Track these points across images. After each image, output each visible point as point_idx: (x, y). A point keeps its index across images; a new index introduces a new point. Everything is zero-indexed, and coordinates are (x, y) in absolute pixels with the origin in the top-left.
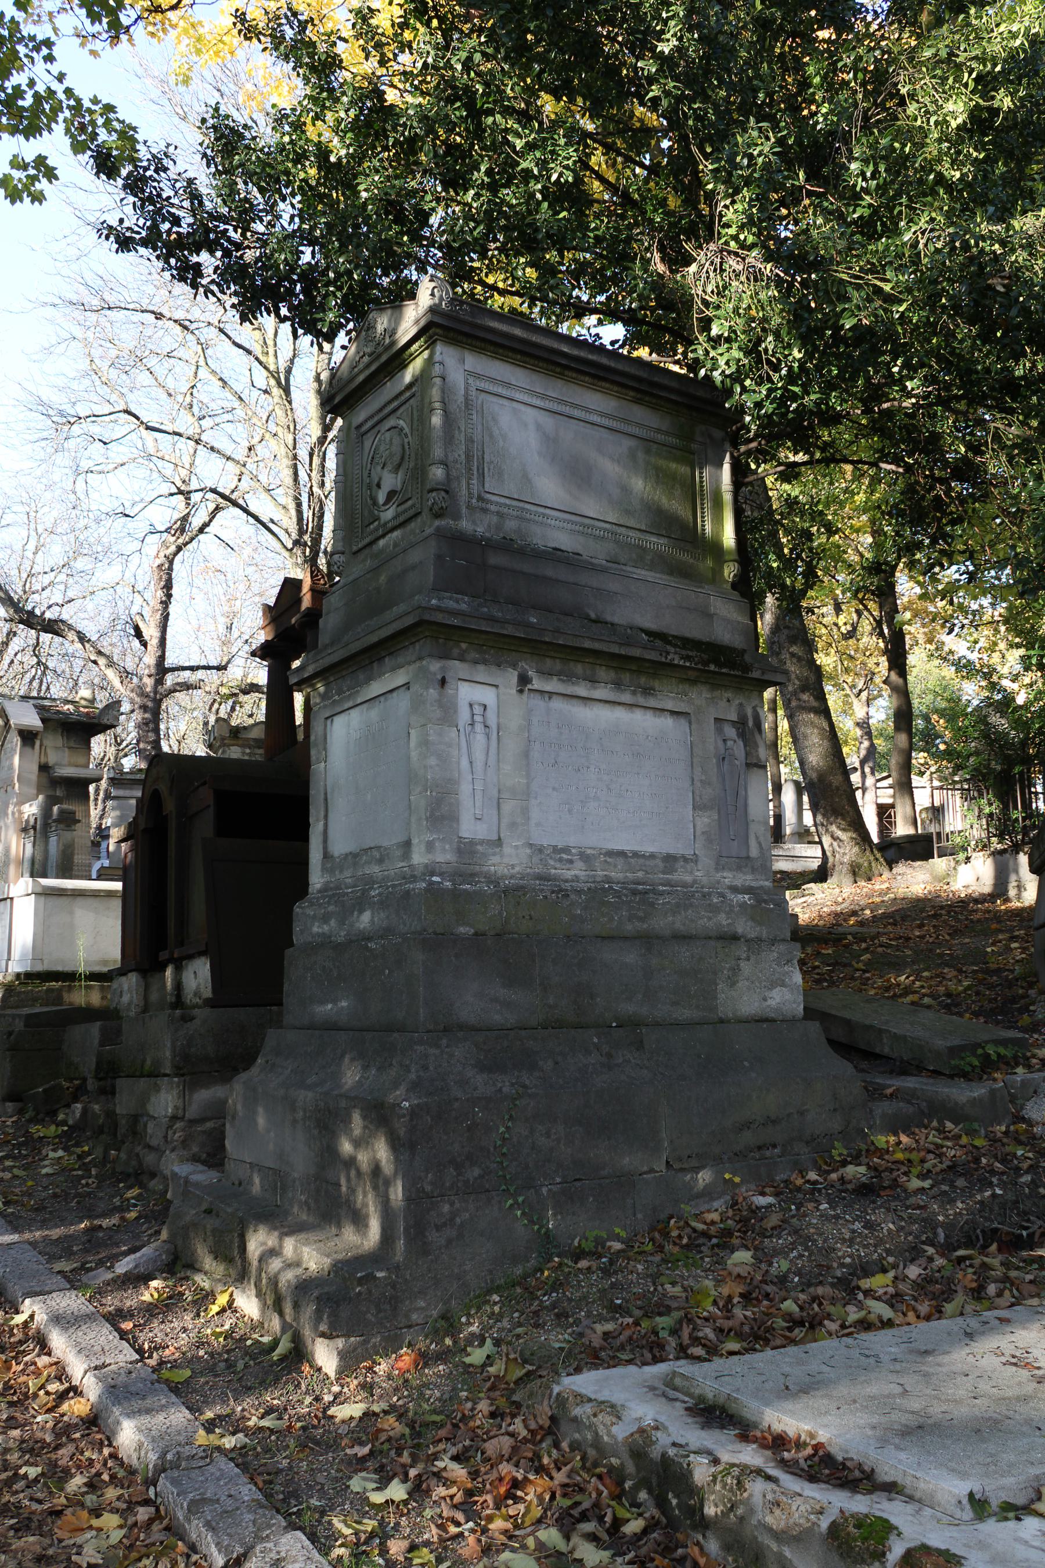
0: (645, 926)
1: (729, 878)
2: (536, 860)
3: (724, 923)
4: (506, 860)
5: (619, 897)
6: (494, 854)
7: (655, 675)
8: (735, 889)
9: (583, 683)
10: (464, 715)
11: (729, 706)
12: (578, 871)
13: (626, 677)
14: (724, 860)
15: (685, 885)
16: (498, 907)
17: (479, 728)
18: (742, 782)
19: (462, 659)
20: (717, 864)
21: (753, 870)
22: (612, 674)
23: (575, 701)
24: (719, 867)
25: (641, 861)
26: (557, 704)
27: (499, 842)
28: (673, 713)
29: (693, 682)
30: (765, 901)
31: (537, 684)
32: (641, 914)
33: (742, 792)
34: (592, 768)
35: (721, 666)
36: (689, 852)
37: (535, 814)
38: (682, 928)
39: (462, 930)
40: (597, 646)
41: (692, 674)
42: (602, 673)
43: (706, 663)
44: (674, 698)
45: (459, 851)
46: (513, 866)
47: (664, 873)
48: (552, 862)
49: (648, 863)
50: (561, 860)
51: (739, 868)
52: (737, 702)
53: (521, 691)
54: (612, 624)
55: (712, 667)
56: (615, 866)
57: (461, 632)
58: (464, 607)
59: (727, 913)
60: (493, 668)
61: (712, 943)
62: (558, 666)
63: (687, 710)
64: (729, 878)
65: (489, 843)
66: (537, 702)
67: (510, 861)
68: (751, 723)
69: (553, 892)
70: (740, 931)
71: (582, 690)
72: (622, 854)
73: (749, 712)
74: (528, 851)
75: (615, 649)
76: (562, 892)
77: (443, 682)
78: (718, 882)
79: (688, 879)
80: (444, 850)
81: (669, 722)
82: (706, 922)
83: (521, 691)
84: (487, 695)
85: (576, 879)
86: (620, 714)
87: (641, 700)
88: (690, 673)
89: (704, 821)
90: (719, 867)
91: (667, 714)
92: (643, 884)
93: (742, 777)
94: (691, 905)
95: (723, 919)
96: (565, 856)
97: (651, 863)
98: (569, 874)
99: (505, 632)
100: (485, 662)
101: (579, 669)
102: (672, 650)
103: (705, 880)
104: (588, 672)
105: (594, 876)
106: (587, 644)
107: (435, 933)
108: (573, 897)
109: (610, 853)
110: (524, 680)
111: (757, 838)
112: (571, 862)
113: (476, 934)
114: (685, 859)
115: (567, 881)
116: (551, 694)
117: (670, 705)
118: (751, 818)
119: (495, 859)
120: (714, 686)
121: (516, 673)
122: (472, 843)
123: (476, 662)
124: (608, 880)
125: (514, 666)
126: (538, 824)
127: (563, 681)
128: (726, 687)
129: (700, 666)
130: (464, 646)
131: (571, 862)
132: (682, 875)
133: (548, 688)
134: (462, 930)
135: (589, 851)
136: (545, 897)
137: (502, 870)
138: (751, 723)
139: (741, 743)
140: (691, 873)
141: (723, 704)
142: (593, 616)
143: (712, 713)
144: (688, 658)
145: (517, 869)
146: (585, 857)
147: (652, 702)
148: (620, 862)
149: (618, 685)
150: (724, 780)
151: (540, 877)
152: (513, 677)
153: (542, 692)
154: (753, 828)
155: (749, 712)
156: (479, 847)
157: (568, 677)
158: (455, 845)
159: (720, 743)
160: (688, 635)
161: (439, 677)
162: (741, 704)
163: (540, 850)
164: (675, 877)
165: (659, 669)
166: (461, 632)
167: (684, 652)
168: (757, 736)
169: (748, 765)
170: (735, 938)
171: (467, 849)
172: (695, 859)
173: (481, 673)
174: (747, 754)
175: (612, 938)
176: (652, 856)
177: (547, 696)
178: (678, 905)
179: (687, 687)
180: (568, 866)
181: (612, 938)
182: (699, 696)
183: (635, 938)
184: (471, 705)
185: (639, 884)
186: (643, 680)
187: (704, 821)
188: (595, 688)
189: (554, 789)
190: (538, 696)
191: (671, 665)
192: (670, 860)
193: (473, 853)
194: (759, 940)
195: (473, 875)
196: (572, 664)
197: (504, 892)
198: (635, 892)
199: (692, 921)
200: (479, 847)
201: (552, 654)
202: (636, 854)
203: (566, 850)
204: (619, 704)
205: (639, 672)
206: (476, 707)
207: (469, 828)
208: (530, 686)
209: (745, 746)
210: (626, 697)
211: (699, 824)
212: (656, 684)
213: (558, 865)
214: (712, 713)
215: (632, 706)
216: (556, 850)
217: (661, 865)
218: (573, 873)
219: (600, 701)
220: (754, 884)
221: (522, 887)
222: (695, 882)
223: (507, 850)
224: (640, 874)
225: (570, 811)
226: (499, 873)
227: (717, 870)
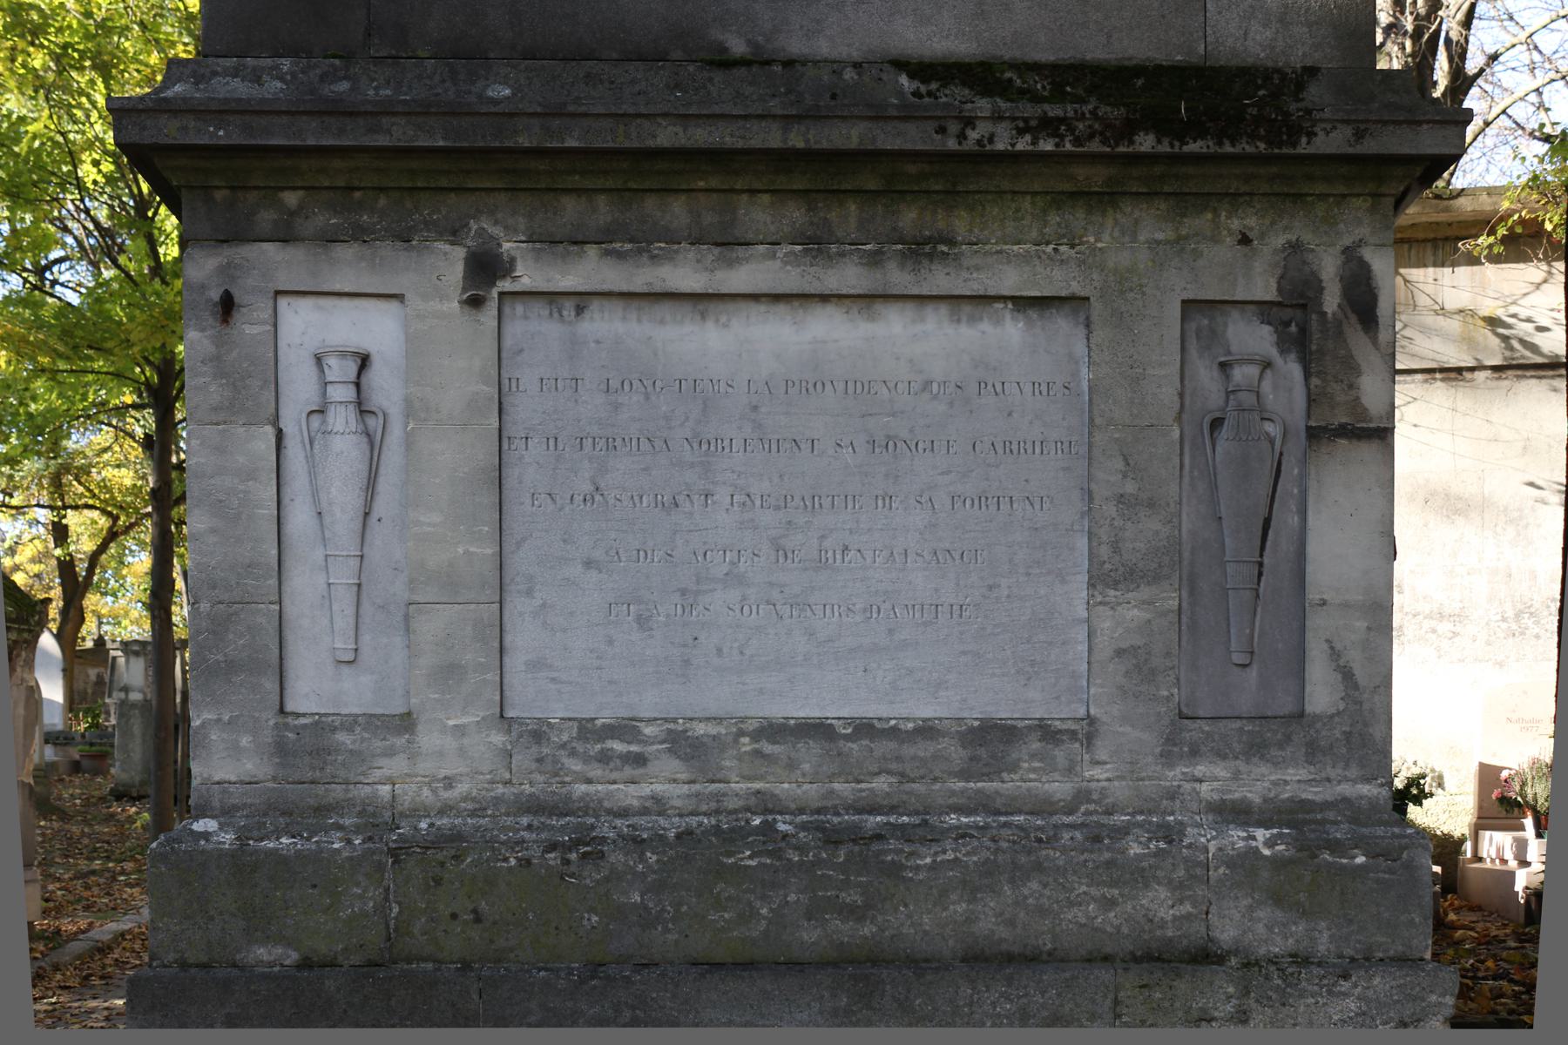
0: (867, 930)
1: (1213, 779)
2: (522, 760)
3: (1166, 913)
4: (425, 767)
5: (776, 854)
6: (390, 753)
7: (952, 197)
8: (1234, 813)
9: (691, 253)
10: (299, 388)
11: (1241, 260)
12: (667, 781)
13: (848, 217)
14: (1194, 731)
15: (1044, 807)
16: (375, 893)
17: (342, 419)
18: (1287, 484)
19: (285, 237)
20: (1170, 740)
21: (1313, 752)
22: (796, 214)
23: (665, 309)
24: (1175, 747)
25: (885, 747)
26: (603, 324)
27: (406, 722)
28: (1022, 303)
29: (1103, 199)
30: (1336, 847)
31: (528, 275)
32: (853, 897)
33: (1285, 519)
34: (722, 495)
35: (1181, 132)
36: (1064, 711)
37: (524, 637)
38: (1003, 932)
39: (262, 953)
40: (701, 136)
41: (1095, 177)
42: (757, 215)
43: (1128, 130)
44: (1026, 258)
45: (281, 750)
46: (449, 782)
47: (965, 775)
48: (575, 766)
49: (908, 750)
50: (605, 758)
51: (1256, 749)
52: (1279, 240)
53: (475, 302)
54: (789, 63)
55: (1146, 143)
56: (792, 765)
57: (283, 163)
58: (273, 87)
59: (1177, 887)
60: (386, 249)
61: (1104, 975)
62: (604, 211)
63: (1076, 288)
64: (1213, 779)
65: (375, 723)
66: (533, 330)
67: (444, 765)
68: (1331, 302)
69: (553, 847)
70: (1226, 933)
71: (684, 275)
72: (818, 730)
73: (1329, 267)
74: (498, 739)
75: (771, 137)
76: (579, 839)
77: (227, 306)
78: (1173, 794)
79: (1059, 788)
80: (235, 751)
81: (1011, 331)
82: (1088, 912)
83: (475, 302)
84: (376, 328)
85: (658, 805)
86: (830, 330)
87: (898, 278)
88: (1081, 172)
89: (1129, 615)
90: (1175, 747)
91: (1006, 311)
92: (893, 809)
93: (1291, 470)
94: (1039, 867)
95: (1161, 906)
96: (618, 746)
97: (924, 749)
98: (631, 794)
99: (382, 141)
100: (360, 235)
101: (677, 212)
102: (983, 106)
103: (1120, 791)
104: (709, 218)
105: (718, 797)
106: (667, 136)
107: (184, 965)
108: (616, 858)
109: (774, 731)
110: (485, 269)
111: (1334, 654)
112: (640, 760)
113: (306, 964)
114: (1047, 732)
115: (624, 813)
116: (582, 300)
117: (1010, 280)
118: (1312, 595)
119: (394, 766)
120: (1185, 201)
121: (459, 253)
122: (322, 726)
123: (330, 239)
124: (768, 805)
125: (454, 234)
126: (536, 665)
127: (620, 256)
128: (1235, 199)
129: (1095, 146)
130: (291, 199)
131: (640, 760)
132: (1034, 779)
133: (569, 278)
134: (262, 953)
135: (700, 729)
136: (526, 863)
137: (409, 793)
138: (1331, 302)
139: (1293, 369)
140: (1070, 770)
141: (1226, 251)
142: (738, 47)
143: (1179, 285)
144: (1048, 126)
145: (462, 788)
146: (682, 743)
147: (940, 279)
148: (809, 754)
149: (815, 244)
150: (1213, 487)
151: (534, 806)
152: (450, 263)
153: (552, 297)
154: (1319, 627)
155: (1329, 267)
156: (342, 737)
157: (642, 241)
158: (268, 737)
159: (1206, 376)
160: (1095, 49)
161: (215, 294)
162: (1295, 247)
163: (538, 733)
164: (1007, 786)
165: (961, 176)
166: (283, 163)
167: (1028, 110)
168: (1357, 340)
169: (1315, 435)
170: (1206, 956)
171: (306, 744)
172: (1088, 732)
173: (347, 266)
174: (1311, 401)
175: (749, 965)
176: (927, 730)
177: (569, 307)
178: (988, 869)
179: (1077, 217)
180: (629, 771)
181: (749, 965)
182: (1127, 241)
183: (823, 964)
184: (318, 360)
185: (873, 810)
186: (909, 218)
187: (1129, 615)
188: (731, 263)
189: (588, 564)
190: (540, 308)
191: (985, 159)
192: (992, 740)
193: (322, 753)
194: (1302, 960)
195: (322, 810)
196: (650, 203)
197: (394, 853)
198: (832, 838)
199: (1042, 911)
200: (342, 737)
201: (576, 180)
202: (865, 729)
203: (625, 729)
204: (824, 298)
205: (892, 194)
206: (332, 361)
207: (314, 688)
208: (506, 285)
209: (1307, 375)
210: (848, 276)
211: (1105, 624)
212: (961, 224)
213: (596, 771)
214: (1179, 285)
215: (868, 300)
216: (587, 729)
217: (957, 754)
218: (646, 789)
219: (755, 297)
220: (1312, 794)
221: (456, 836)
222: (1082, 796)
223: (428, 739)
224: (881, 784)
225: (643, 622)
226: (406, 802)
227: (1167, 758)
